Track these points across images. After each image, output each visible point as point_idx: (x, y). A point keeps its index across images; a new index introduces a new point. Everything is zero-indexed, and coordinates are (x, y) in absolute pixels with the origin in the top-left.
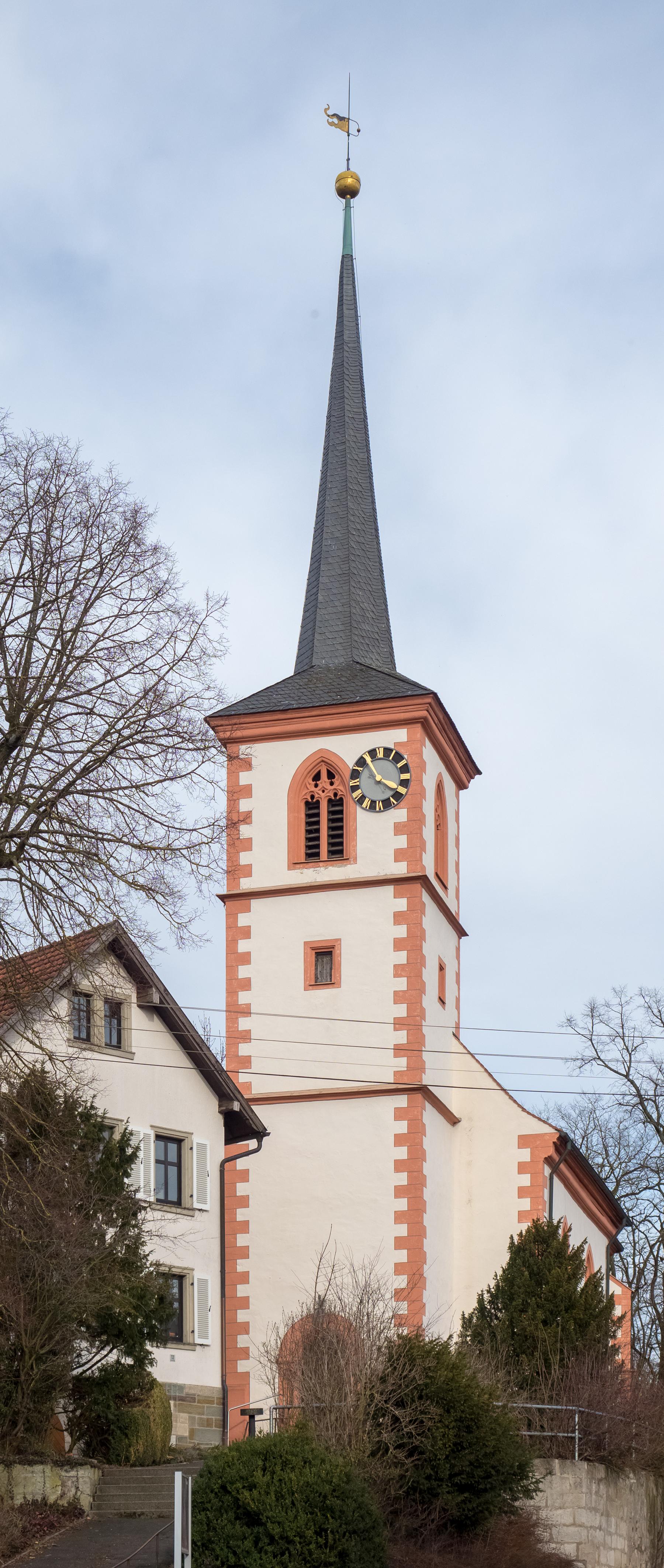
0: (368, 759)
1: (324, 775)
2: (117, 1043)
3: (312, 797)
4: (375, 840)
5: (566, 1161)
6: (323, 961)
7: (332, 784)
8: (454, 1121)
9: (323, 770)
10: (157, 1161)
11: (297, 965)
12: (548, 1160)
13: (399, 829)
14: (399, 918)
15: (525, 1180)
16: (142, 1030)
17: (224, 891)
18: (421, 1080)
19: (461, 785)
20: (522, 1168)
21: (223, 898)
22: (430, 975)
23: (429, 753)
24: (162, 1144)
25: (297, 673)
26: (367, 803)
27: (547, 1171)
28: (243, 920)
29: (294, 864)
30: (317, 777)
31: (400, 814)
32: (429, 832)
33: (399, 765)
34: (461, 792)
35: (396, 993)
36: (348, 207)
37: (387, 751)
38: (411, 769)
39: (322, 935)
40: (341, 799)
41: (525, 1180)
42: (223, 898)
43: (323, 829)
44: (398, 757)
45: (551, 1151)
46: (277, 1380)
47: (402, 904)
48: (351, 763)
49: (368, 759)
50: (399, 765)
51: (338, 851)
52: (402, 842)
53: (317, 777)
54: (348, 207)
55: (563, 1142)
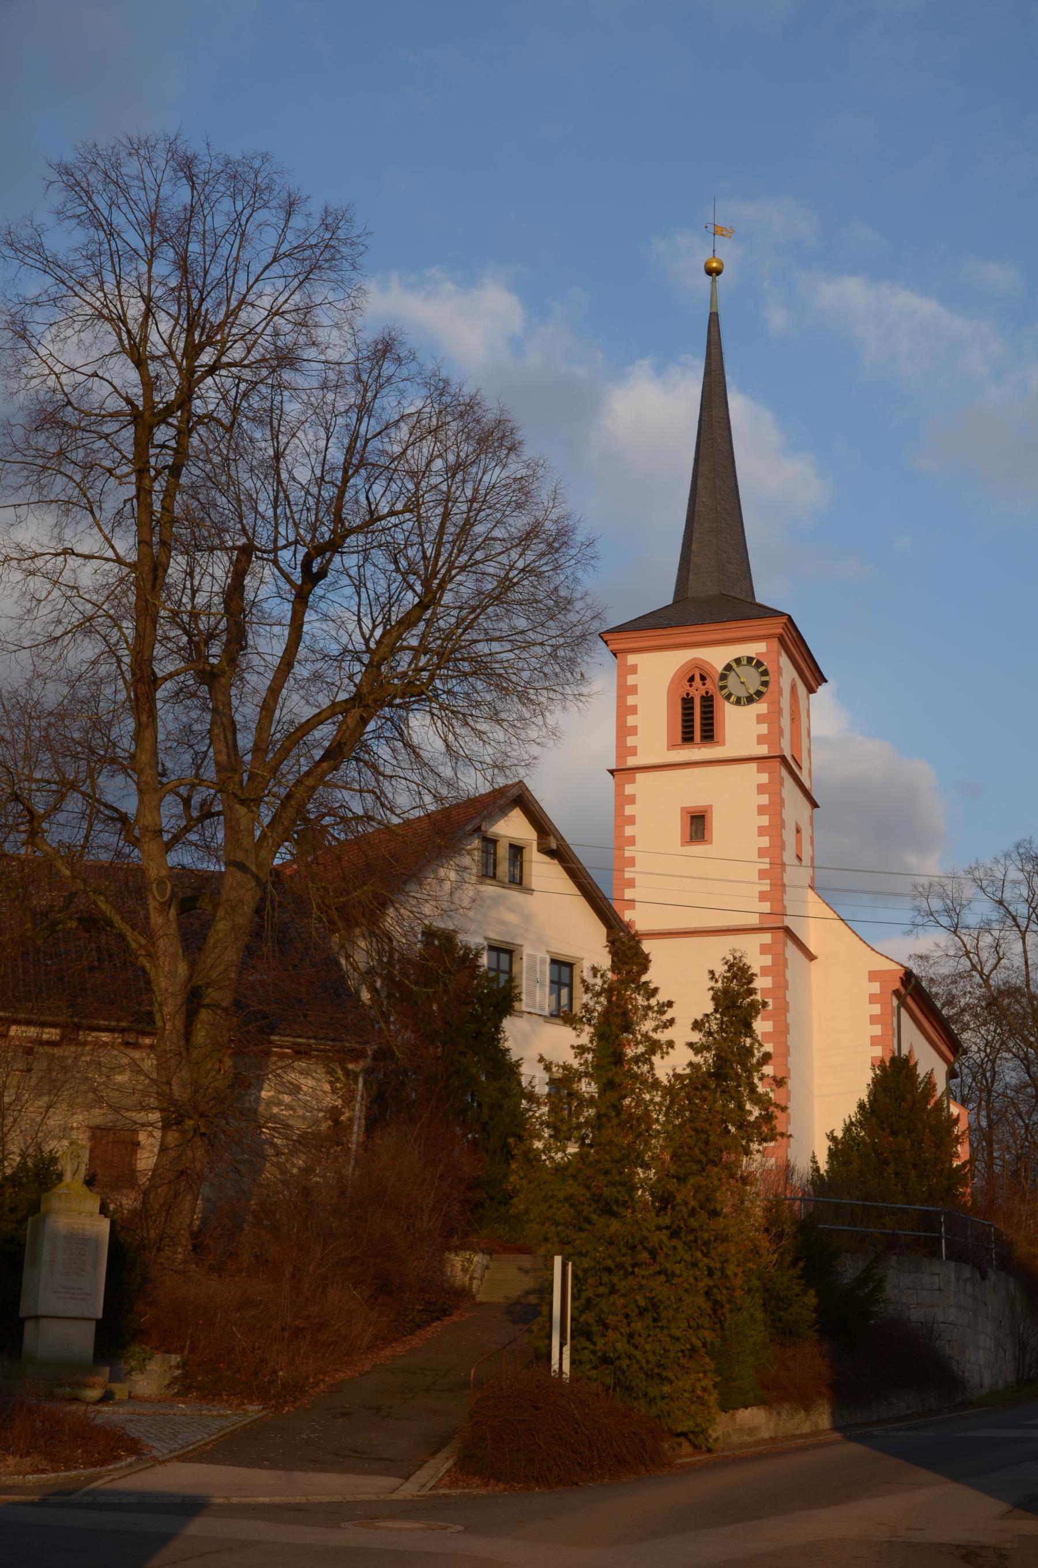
0: (734, 665)
1: (697, 678)
2: (518, 881)
3: (688, 694)
4: (741, 727)
5: (910, 995)
6: (697, 825)
7: (704, 684)
8: (811, 957)
9: (696, 674)
10: (552, 982)
11: (675, 827)
12: (896, 993)
13: (760, 719)
14: (761, 789)
15: (876, 1009)
16: (543, 871)
17: (613, 767)
18: (783, 922)
19: (811, 690)
20: (873, 999)
21: (611, 772)
22: (789, 836)
23: (784, 660)
24: (556, 967)
25: (676, 601)
26: (732, 699)
27: (895, 1002)
28: (629, 789)
29: (672, 746)
30: (691, 679)
31: (761, 707)
32: (785, 722)
33: (761, 670)
34: (811, 696)
35: (760, 849)
36: (714, 281)
37: (750, 660)
38: (770, 673)
39: (696, 801)
40: (712, 696)
41: (876, 1009)
42: (611, 772)
43: (697, 719)
44: (759, 664)
45: (897, 985)
46: (110, 1467)
47: (764, 778)
48: (720, 668)
49: (734, 665)
50: (761, 670)
51: (709, 735)
52: (764, 729)
53: (691, 679)
54: (714, 281)
55: (908, 977)
